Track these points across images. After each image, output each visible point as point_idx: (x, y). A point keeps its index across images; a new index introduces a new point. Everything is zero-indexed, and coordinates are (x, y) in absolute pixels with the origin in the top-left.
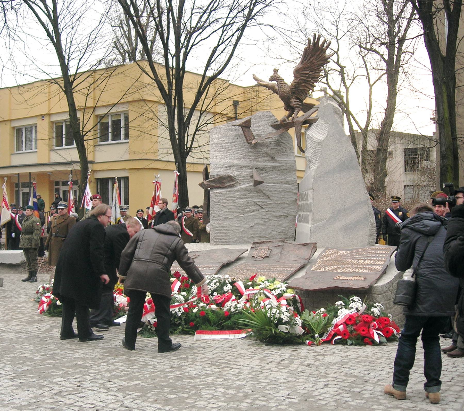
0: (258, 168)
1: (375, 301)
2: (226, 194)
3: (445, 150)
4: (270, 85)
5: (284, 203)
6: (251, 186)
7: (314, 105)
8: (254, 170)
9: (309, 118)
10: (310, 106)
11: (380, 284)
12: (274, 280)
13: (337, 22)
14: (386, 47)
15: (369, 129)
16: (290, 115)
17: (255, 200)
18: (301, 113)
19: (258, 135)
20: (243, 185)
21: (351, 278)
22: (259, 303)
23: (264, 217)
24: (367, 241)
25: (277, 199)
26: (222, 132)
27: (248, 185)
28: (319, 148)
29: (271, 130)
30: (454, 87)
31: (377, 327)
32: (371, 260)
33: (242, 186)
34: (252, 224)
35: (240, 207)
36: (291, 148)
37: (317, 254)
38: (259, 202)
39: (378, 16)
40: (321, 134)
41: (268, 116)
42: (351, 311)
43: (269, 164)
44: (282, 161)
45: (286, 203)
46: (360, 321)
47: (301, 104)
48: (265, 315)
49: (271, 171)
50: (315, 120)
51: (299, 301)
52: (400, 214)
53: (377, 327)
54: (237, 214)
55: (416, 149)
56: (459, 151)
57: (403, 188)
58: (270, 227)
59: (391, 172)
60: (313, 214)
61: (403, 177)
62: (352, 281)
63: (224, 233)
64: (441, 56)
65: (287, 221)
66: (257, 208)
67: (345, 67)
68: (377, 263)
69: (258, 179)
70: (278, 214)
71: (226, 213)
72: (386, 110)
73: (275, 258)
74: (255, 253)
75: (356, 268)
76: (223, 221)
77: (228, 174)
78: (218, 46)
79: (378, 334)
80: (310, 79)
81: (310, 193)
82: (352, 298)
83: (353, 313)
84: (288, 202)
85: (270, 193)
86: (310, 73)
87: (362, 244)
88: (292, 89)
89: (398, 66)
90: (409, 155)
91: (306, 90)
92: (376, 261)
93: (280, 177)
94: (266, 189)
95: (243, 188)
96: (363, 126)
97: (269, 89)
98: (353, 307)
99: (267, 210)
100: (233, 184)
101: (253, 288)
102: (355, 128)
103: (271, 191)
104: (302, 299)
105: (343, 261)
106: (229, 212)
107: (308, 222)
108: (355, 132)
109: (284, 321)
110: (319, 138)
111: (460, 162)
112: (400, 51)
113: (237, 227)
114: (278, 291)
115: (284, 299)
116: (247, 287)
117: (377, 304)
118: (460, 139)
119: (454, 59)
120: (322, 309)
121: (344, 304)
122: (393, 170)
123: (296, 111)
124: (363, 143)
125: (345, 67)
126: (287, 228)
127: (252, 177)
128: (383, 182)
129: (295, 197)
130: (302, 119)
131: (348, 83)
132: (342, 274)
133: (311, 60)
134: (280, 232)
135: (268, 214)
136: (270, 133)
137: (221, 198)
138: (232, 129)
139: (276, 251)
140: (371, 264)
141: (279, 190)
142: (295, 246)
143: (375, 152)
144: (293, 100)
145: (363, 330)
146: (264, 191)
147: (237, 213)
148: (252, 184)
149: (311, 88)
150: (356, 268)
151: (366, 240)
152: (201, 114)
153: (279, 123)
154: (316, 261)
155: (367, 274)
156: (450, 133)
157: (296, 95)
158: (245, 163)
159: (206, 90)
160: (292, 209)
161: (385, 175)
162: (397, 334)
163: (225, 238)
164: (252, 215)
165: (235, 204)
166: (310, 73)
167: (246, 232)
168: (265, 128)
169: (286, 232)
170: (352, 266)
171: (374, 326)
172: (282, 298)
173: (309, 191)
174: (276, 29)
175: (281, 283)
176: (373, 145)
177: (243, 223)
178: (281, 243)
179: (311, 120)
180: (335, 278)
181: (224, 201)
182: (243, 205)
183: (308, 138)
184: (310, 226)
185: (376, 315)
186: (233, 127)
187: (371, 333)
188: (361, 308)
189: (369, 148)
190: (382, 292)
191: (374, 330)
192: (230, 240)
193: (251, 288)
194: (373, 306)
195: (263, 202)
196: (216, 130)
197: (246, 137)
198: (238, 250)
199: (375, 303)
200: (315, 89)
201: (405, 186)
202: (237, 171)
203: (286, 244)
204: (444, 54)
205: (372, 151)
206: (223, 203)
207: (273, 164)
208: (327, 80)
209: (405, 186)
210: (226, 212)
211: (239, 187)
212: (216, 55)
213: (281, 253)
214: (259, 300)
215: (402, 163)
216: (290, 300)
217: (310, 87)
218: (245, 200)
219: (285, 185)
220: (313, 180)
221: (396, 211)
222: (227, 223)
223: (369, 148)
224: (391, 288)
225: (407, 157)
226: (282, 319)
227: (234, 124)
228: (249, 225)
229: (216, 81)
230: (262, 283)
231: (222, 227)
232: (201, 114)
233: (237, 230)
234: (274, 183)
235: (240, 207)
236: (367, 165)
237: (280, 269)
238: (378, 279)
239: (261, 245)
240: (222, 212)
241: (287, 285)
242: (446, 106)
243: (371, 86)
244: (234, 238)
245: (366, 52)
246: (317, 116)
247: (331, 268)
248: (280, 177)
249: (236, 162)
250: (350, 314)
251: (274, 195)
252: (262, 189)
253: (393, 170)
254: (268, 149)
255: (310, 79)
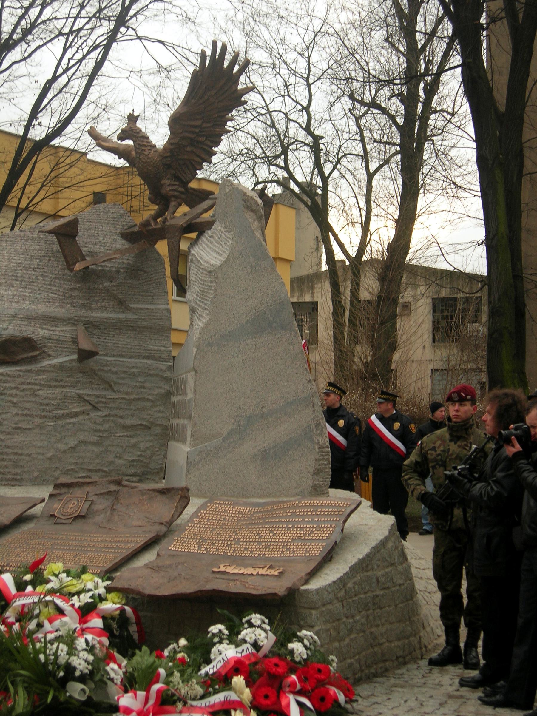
0: (91, 323)
1: (302, 623)
2: (19, 376)
3: (499, 299)
4: (121, 148)
5: (143, 399)
6: (72, 361)
7: (212, 193)
8: (81, 328)
9: (198, 220)
10: (204, 195)
11: (314, 585)
12: (84, 570)
13: (310, 51)
14: (401, 101)
15: (364, 258)
16: (160, 214)
17: (81, 392)
18: (184, 209)
19: (92, 254)
20: (55, 357)
21: (250, 571)
22: (40, 626)
23: (99, 427)
24: (310, 483)
25: (129, 390)
26: (19, 246)
27: (67, 358)
28: (211, 282)
29: (121, 244)
30: (520, 174)
31: (299, 687)
32: (302, 529)
33: (55, 361)
34: (73, 442)
35: (47, 404)
36: (162, 284)
37: (190, 510)
38: (88, 395)
39: (387, 40)
40: (218, 253)
41: (115, 215)
42: (240, 649)
43: (113, 315)
44: (141, 309)
45: (148, 400)
46: (260, 674)
47: (183, 190)
48: (36, 659)
49: (118, 331)
50: (209, 225)
51: (134, 620)
52: (397, 425)
53: (299, 687)
54: (38, 421)
55: (455, 299)
56: (527, 301)
57: (430, 372)
58: (110, 448)
59: (404, 342)
60: (195, 424)
61: (428, 353)
62: (251, 578)
63: (10, 460)
64: (496, 110)
65: (148, 438)
66: (85, 408)
67: (322, 138)
68: (314, 536)
69: (85, 345)
70: (129, 422)
71: (17, 418)
72: (397, 222)
73: (99, 519)
74: (57, 506)
75: (267, 547)
76: (9, 434)
77: (25, 334)
78: (55, 78)
79: (300, 704)
80: (202, 139)
81: (190, 378)
82: (247, 618)
83: (244, 654)
84: (150, 397)
85: (114, 377)
86: (204, 125)
87: (299, 490)
88: (166, 157)
89: (423, 138)
90: (442, 311)
91: (194, 161)
92: (312, 532)
93: (136, 343)
94: (106, 368)
95: (54, 366)
96: (353, 253)
97: (119, 158)
98: (247, 639)
99: (106, 412)
100: (33, 357)
101: (35, 588)
102: (339, 256)
103: (116, 373)
104: (141, 614)
105: (240, 529)
106: (23, 415)
107: (184, 441)
108: (338, 265)
109: (77, 674)
110: (212, 262)
111: (529, 325)
112: (428, 109)
113: (39, 447)
114: (86, 598)
115: (99, 616)
116: (21, 586)
117: (304, 632)
118: (529, 277)
119: (522, 118)
120: (183, 642)
121: (226, 632)
122: (408, 339)
123: (173, 204)
124: (352, 285)
125: (322, 138)
126: (149, 452)
127: (75, 341)
128: (389, 361)
129: (167, 387)
130: (181, 222)
131: (327, 169)
132: (235, 560)
133: (206, 97)
134: (133, 461)
135: (108, 421)
136: (117, 251)
137: (8, 385)
138: (39, 239)
139: (102, 504)
140: (300, 538)
141: (134, 370)
142: (143, 495)
143: (375, 305)
144: (166, 182)
145: (266, 697)
146: (100, 373)
147: (41, 417)
148: (75, 356)
149: (206, 157)
150: (267, 547)
151: (308, 481)
152: (17, 216)
153: (136, 229)
154: (182, 528)
155: (289, 561)
156: (509, 265)
157: (173, 172)
158: (61, 312)
159: (30, 166)
160: (159, 411)
161: (393, 347)
162: (346, 702)
163: (13, 471)
164: (74, 424)
165: (37, 399)
166: (204, 125)
167: (60, 459)
168: (108, 240)
169: (147, 461)
170: (259, 543)
171: (293, 684)
172: (94, 614)
173: (189, 375)
174: (171, 49)
175: (96, 579)
176: (371, 290)
177: (53, 439)
178: (113, 488)
179: (201, 223)
180: (216, 570)
181: (14, 392)
182: (55, 402)
183: (192, 261)
184: (188, 449)
185: (298, 659)
186: (42, 235)
187: (284, 703)
188: (265, 641)
189: (364, 295)
190: (320, 604)
191: (291, 697)
192: (25, 476)
193: (29, 588)
194: (293, 637)
195: (98, 396)
196: (6, 241)
197: (65, 257)
198: (22, 501)
199: (301, 628)
200: (214, 159)
201: (432, 370)
202: (43, 329)
203: (125, 490)
204: (502, 108)
205: (369, 302)
206: (11, 395)
207: (121, 316)
208: (286, 161)
209: (432, 370)
210: (17, 414)
211: (46, 363)
212: (49, 96)
213: (113, 509)
214: (42, 618)
215: (428, 326)
216: (113, 618)
217: (203, 156)
218: (58, 390)
219: (145, 361)
220: (195, 350)
221: (387, 421)
222: (18, 438)
223: (364, 295)
224: (342, 594)
225: (438, 314)
226: (75, 669)
227: (43, 229)
228: (66, 444)
229: (45, 151)
230: (52, 578)
231: (8, 447)
232: (17, 216)
233: (39, 454)
234: (122, 356)
235: (47, 404)
236: (360, 329)
237: (103, 545)
238: (312, 574)
239: (71, 490)
240: (9, 415)
241: (109, 582)
242: (502, 213)
243: (370, 176)
244: (33, 471)
245: (364, 109)
246: (214, 216)
247: (213, 544)
248: (136, 343)
249: (42, 309)
250: (239, 655)
251: (121, 381)
252: (96, 368)
253: (408, 339)
254: (113, 284)
255: (202, 139)
